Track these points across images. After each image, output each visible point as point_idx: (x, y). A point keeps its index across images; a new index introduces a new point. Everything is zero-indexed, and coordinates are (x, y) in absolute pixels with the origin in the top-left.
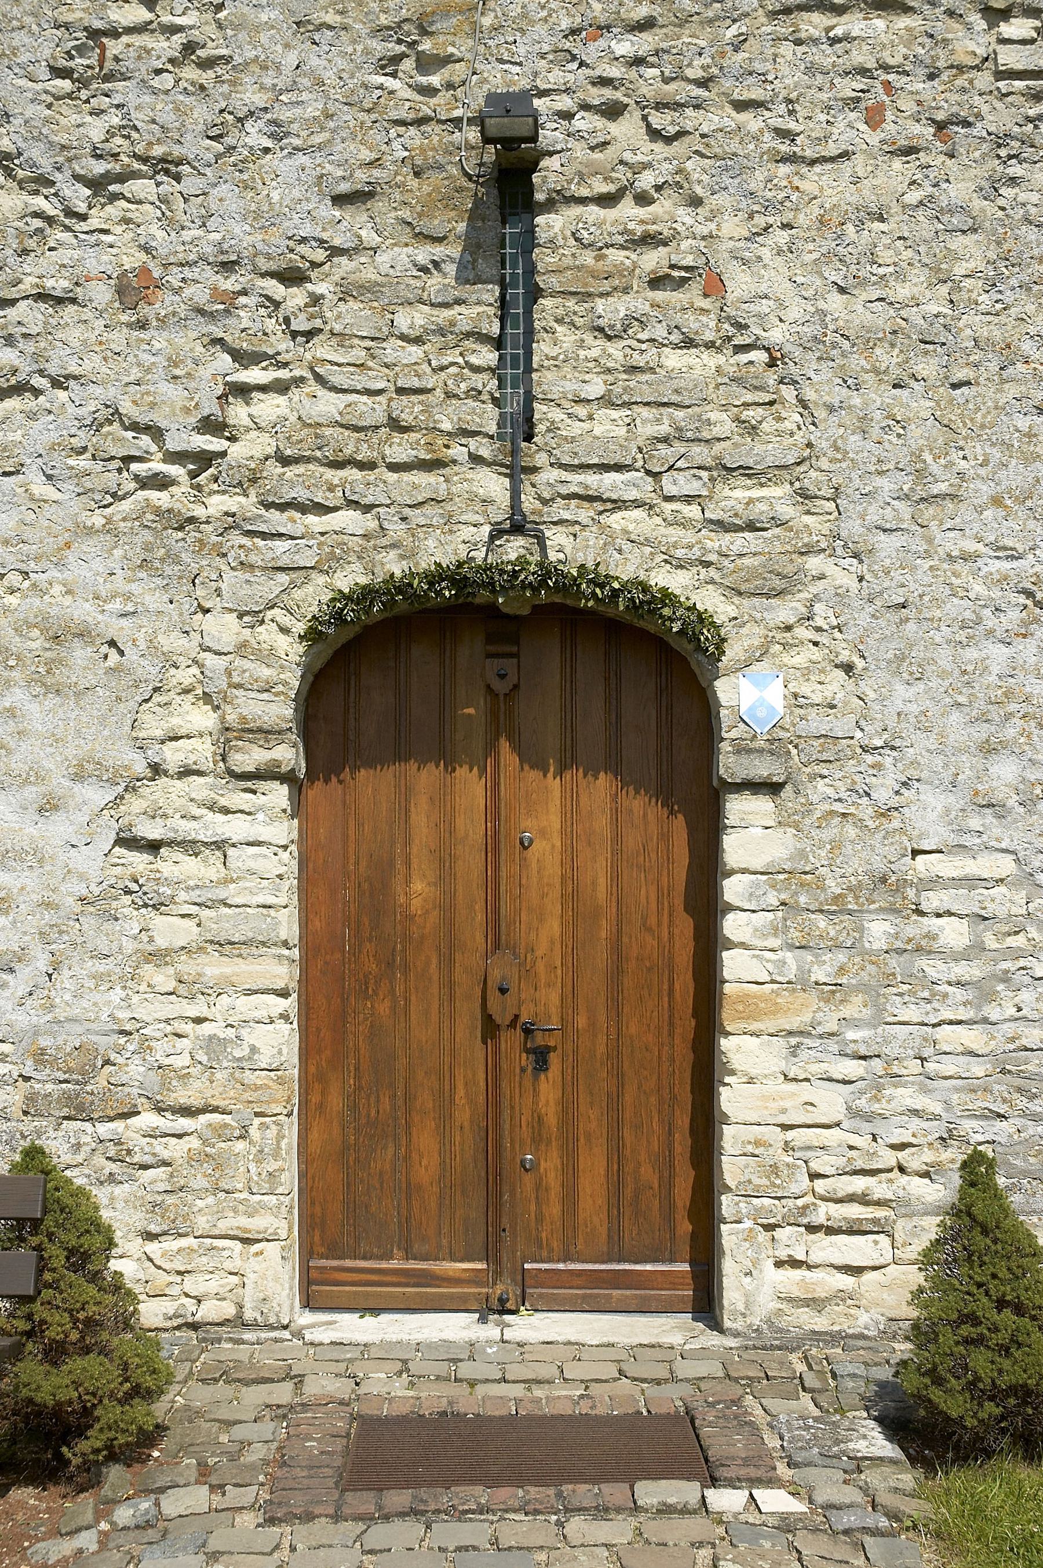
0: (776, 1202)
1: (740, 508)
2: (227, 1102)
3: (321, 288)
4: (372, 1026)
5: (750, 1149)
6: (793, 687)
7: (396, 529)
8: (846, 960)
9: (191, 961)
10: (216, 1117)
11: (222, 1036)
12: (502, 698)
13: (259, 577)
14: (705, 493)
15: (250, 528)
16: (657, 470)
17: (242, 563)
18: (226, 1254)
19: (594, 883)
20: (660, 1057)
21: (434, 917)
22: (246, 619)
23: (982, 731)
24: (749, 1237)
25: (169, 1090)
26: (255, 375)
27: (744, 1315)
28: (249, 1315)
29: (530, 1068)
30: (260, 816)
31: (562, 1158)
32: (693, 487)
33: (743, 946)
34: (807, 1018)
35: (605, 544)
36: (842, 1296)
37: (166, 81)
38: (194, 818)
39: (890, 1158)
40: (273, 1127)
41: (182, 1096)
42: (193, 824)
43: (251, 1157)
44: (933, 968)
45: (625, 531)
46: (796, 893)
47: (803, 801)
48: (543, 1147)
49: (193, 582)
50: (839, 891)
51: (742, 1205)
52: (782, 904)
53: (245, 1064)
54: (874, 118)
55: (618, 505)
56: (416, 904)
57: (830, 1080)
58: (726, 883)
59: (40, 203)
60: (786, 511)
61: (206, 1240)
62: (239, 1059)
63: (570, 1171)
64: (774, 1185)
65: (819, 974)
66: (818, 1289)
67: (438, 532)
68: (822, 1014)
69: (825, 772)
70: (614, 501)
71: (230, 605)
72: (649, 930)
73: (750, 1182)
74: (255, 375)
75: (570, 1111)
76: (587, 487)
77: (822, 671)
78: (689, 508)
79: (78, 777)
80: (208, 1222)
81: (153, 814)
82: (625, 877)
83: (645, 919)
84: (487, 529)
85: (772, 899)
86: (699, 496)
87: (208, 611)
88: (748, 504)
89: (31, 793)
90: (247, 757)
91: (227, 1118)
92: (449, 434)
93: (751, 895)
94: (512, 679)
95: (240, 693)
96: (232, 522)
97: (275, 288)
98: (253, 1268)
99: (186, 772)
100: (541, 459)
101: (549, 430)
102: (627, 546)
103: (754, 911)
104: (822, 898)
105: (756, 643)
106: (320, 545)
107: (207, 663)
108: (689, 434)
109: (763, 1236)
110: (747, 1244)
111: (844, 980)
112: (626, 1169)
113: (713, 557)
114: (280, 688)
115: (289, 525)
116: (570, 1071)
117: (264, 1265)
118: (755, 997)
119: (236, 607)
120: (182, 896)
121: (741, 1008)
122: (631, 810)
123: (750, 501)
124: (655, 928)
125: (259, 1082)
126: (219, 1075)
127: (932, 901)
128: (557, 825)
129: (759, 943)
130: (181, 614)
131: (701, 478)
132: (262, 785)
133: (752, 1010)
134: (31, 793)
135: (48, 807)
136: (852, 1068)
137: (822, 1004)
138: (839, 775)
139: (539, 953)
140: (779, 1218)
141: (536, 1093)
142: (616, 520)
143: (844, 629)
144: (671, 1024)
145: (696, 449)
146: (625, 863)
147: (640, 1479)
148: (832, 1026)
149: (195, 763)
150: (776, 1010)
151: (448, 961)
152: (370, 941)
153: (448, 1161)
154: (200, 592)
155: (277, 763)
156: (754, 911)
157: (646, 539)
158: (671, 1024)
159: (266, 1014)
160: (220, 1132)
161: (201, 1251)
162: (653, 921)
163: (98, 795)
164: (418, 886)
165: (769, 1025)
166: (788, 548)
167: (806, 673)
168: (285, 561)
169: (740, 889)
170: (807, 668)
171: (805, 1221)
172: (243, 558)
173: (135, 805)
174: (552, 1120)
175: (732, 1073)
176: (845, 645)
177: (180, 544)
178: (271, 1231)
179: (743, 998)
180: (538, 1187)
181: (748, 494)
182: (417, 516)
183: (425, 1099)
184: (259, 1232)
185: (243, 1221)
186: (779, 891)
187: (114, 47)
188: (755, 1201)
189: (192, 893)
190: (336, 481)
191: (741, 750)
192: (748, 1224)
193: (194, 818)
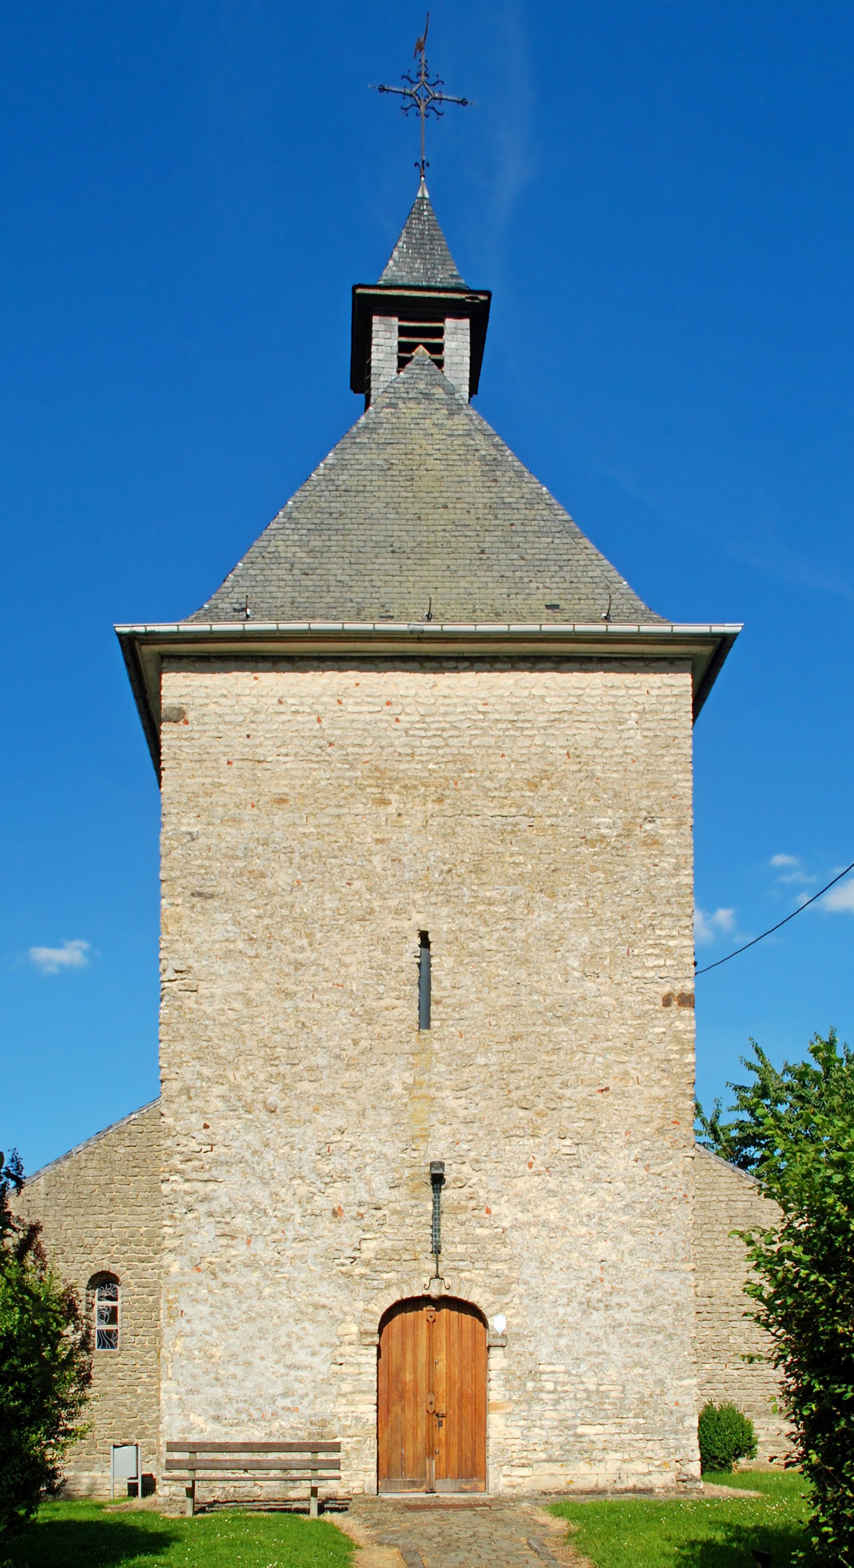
3: (386, 1212)
7: (406, 1277)
21: (412, 1384)
23: (557, 1331)
26: (368, 1236)
32: (483, 1266)
36: (520, 1485)
37: (346, 1156)
39: (531, 1448)
41: (349, 1433)
44: (543, 1396)
54: (530, 1165)
55: (462, 1271)
59: (311, 1189)
60: (506, 1272)
63: (448, 1454)
65: (514, 1398)
74: (368, 1236)
79: (322, 1345)
81: (341, 1355)
85: (503, 1377)
89: (309, 1350)
96: (362, 1276)
97: (374, 1212)
99: (350, 1344)
127: (544, 1377)
133: (497, 1407)
134: (309, 1350)
135: (314, 1354)
136: (522, 1423)
142: (463, 1275)
147: (450, 317)
150: (503, 1408)
151: (415, 1396)
160: (359, 1442)
163: (326, 1350)
165: (501, 1411)
167: (512, 1316)
173: (337, 1353)
174: (443, 1440)
179: (495, 1404)
182: (411, 1274)
183: (410, 1435)
187: (332, 1147)
191: (495, 1336)
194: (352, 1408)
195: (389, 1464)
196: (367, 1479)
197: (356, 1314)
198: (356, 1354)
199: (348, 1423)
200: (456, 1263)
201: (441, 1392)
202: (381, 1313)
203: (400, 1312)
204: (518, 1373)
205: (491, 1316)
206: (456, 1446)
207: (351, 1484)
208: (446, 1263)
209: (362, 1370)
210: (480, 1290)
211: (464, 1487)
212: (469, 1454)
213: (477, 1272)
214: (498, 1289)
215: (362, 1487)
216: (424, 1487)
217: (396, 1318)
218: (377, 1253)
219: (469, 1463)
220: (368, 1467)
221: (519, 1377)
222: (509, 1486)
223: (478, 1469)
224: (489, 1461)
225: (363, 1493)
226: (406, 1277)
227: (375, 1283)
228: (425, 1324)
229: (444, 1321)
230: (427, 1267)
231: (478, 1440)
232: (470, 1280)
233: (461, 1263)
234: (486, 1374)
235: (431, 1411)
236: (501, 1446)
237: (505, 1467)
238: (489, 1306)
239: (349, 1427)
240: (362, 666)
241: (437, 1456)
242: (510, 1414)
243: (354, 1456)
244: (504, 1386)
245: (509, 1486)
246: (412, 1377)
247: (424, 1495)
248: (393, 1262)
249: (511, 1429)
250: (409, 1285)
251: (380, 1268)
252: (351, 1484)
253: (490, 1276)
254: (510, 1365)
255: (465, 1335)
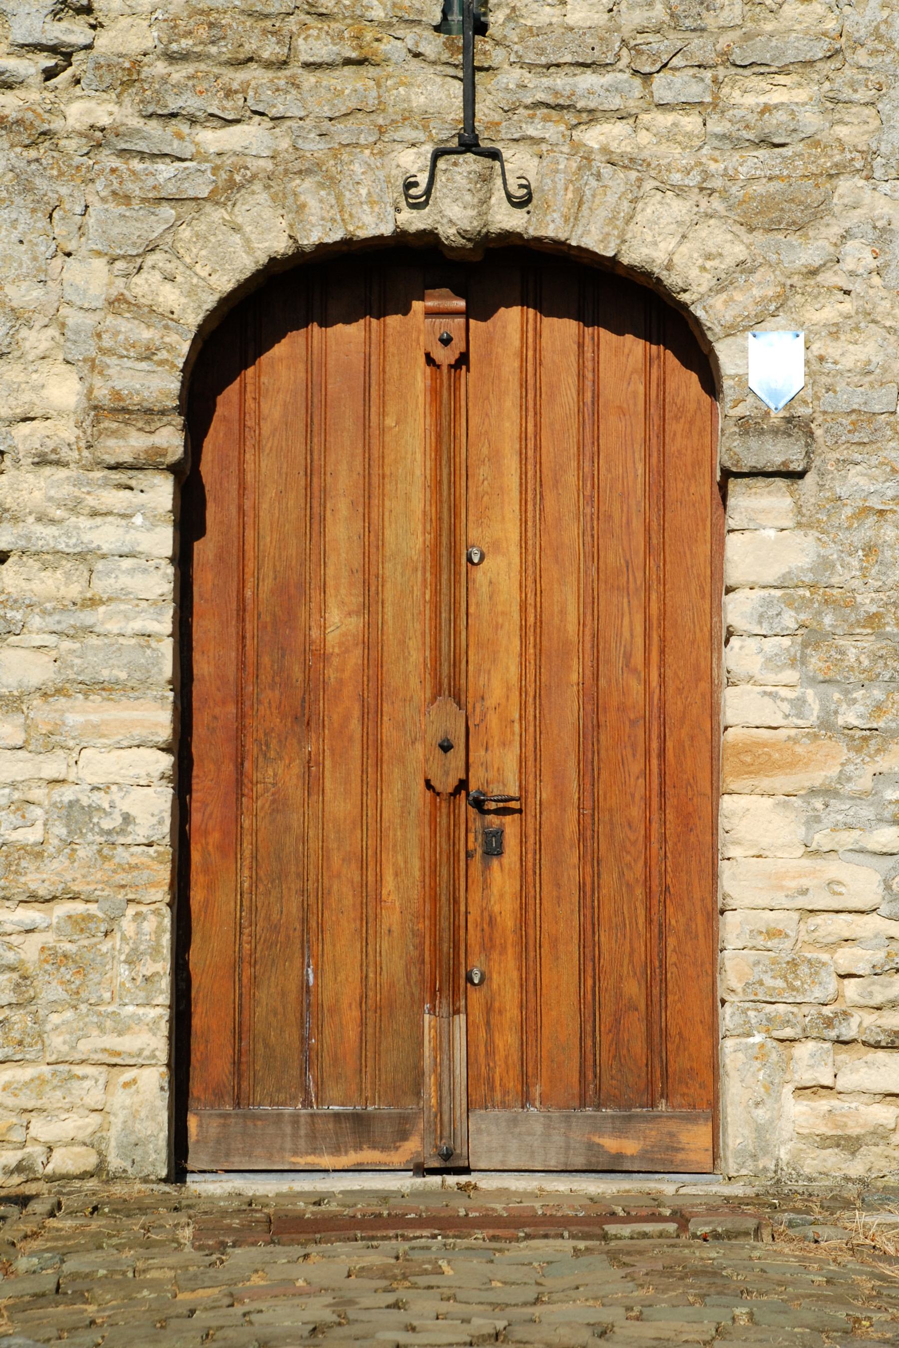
0: (795, 1009)
1: (752, 118)
2: (92, 887)
4: (274, 801)
5: (760, 941)
6: (817, 348)
7: (314, 146)
8: (882, 697)
9: (46, 708)
10: (78, 907)
11: (85, 802)
12: (445, 369)
13: (137, 210)
14: (708, 99)
15: (124, 146)
16: (647, 69)
17: (114, 193)
18: (87, 1084)
19: (563, 612)
20: (647, 837)
21: (355, 657)
22: (120, 265)
24: (760, 1054)
25: (16, 872)
27: (754, 1157)
28: (115, 1162)
29: (479, 851)
30: (138, 520)
31: (520, 969)
32: (695, 91)
33: (750, 679)
34: (833, 772)
35: (579, 169)
38: (52, 521)
40: (152, 918)
42: (52, 530)
43: (123, 958)
45: (605, 150)
46: (819, 613)
47: (828, 494)
48: (495, 955)
49: (51, 217)
50: (873, 609)
51: (752, 1014)
52: (801, 626)
53: (114, 838)
55: (592, 116)
56: (332, 637)
57: (862, 851)
58: (729, 600)
60: (811, 120)
61: (61, 1067)
62: (109, 832)
64: (793, 988)
65: (850, 717)
66: (850, 1123)
67: (367, 152)
68: (852, 767)
69: (857, 457)
70: (591, 111)
71: (99, 247)
72: (635, 671)
73: (761, 983)
75: (531, 908)
76: (556, 93)
77: (857, 328)
78: (687, 119)
80: (65, 1043)
82: (602, 603)
83: (628, 656)
84: (428, 149)
85: (789, 620)
86: (701, 103)
87: (69, 255)
88: (762, 112)
90: (121, 443)
91: (93, 908)
92: (381, 24)
93: (761, 616)
94: (458, 345)
95: (112, 361)
98: (120, 1099)
99: (42, 461)
100: (498, 56)
101: (508, 18)
102: (607, 170)
103: (765, 636)
104: (853, 618)
105: (771, 293)
106: (216, 169)
107: (70, 322)
108: (688, 22)
109: (775, 1052)
110: (757, 1064)
111: (881, 724)
112: (604, 984)
113: (717, 183)
114: (163, 355)
115: (176, 143)
116: (530, 856)
117: (136, 1099)
118: (764, 745)
119: (106, 249)
120: (36, 621)
121: (748, 759)
122: (610, 516)
123: (767, 109)
124: (640, 667)
125: (133, 861)
126: (81, 853)
128: (514, 535)
129: (771, 677)
130: (35, 259)
131: (702, 80)
132: (139, 479)
137: (852, 755)
138: (874, 461)
139: (490, 702)
140: (799, 1030)
141: (486, 885)
143: (883, 273)
144: (662, 794)
145: (696, 42)
146: (602, 586)
148: (865, 782)
149: (54, 451)
150: (792, 764)
152: (272, 687)
153: (371, 975)
154: (59, 230)
155: (160, 452)
156: (765, 636)
157: (631, 160)
158: (662, 794)
159: (143, 773)
160: (81, 924)
161: (55, 1082)
162: (638, 659)
164: (334, 616)
165: (782, 782)
166: (813, 168)
167: (834, 332)
168: (170, 190)
169: (747, 609)
170: (836, 324)
171: (833, 1034)
172: (116, 185)
174: (508, 920)
175: (737, 843)
176: (884, 293)
177: (34, 166)
178: (146, 1053)
179: (749, 748)
180: (489, 1009)
181: (763, 99)
182: (342, 132)
184: (130, 1055)
185: (112, 1041)
186: (797, 610)
188: (769, 1008)
189: (48, 619)
190: (235, 86)
192: (758, 1039)
193: (52, 521)
194: (53, 767)
195: (239, 1032)
196: (120, 1099)
197: (73, 318)
198: (75, 506)
199: (32, 835)
200: (560, 81)
201: (496, 693)
202: (193, 319)
203: (303, 323)
204: (867, 602)
205: (731, 331)
206: (570, 952)
207: (41, 1129)
208: (511, 77)
209: (102, 586)
210: (679, 208)
211: (611, 1144)
212: (633, 989)
213: (664, 120)
214: (768, 203)
215: (94, 1143)
216: (412, 1147)
217: (280, 350)
218: (174, 29)
219: (635, 1026)
220: (128, 1043)
221: (873, 620)
222: (826, 1142)
223: (678, 1063)
224: (728, 1018)
225: (99, 1171)
226: (314, 146)
227: (165, 170)
228: (420, 376)
229: (510, 366)
230: (419, 100)
231: (676, 920)
232: (631, 162)
233: (588, 80)
234: (717, 609)
235: (447, 784)
236: (784, 948)
237: (804, 1050)
238: (721, 285)
239: (37, 852)
240: (719, 704)
241: (476, 997)
242: (828, 792)
243: (53, 991)
244: (797, 661)
245: (826, 1142)
246: (355, 624)
247: (406, 1182)
248: (254, 74)
249: (833, 869)
250: (331, 182)
251: (190, 103)
252: (41, 1129)
253: (736, 143)
254: (825, 564)
255: (611, 424)
